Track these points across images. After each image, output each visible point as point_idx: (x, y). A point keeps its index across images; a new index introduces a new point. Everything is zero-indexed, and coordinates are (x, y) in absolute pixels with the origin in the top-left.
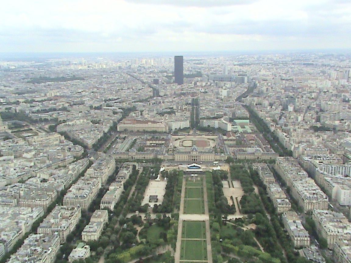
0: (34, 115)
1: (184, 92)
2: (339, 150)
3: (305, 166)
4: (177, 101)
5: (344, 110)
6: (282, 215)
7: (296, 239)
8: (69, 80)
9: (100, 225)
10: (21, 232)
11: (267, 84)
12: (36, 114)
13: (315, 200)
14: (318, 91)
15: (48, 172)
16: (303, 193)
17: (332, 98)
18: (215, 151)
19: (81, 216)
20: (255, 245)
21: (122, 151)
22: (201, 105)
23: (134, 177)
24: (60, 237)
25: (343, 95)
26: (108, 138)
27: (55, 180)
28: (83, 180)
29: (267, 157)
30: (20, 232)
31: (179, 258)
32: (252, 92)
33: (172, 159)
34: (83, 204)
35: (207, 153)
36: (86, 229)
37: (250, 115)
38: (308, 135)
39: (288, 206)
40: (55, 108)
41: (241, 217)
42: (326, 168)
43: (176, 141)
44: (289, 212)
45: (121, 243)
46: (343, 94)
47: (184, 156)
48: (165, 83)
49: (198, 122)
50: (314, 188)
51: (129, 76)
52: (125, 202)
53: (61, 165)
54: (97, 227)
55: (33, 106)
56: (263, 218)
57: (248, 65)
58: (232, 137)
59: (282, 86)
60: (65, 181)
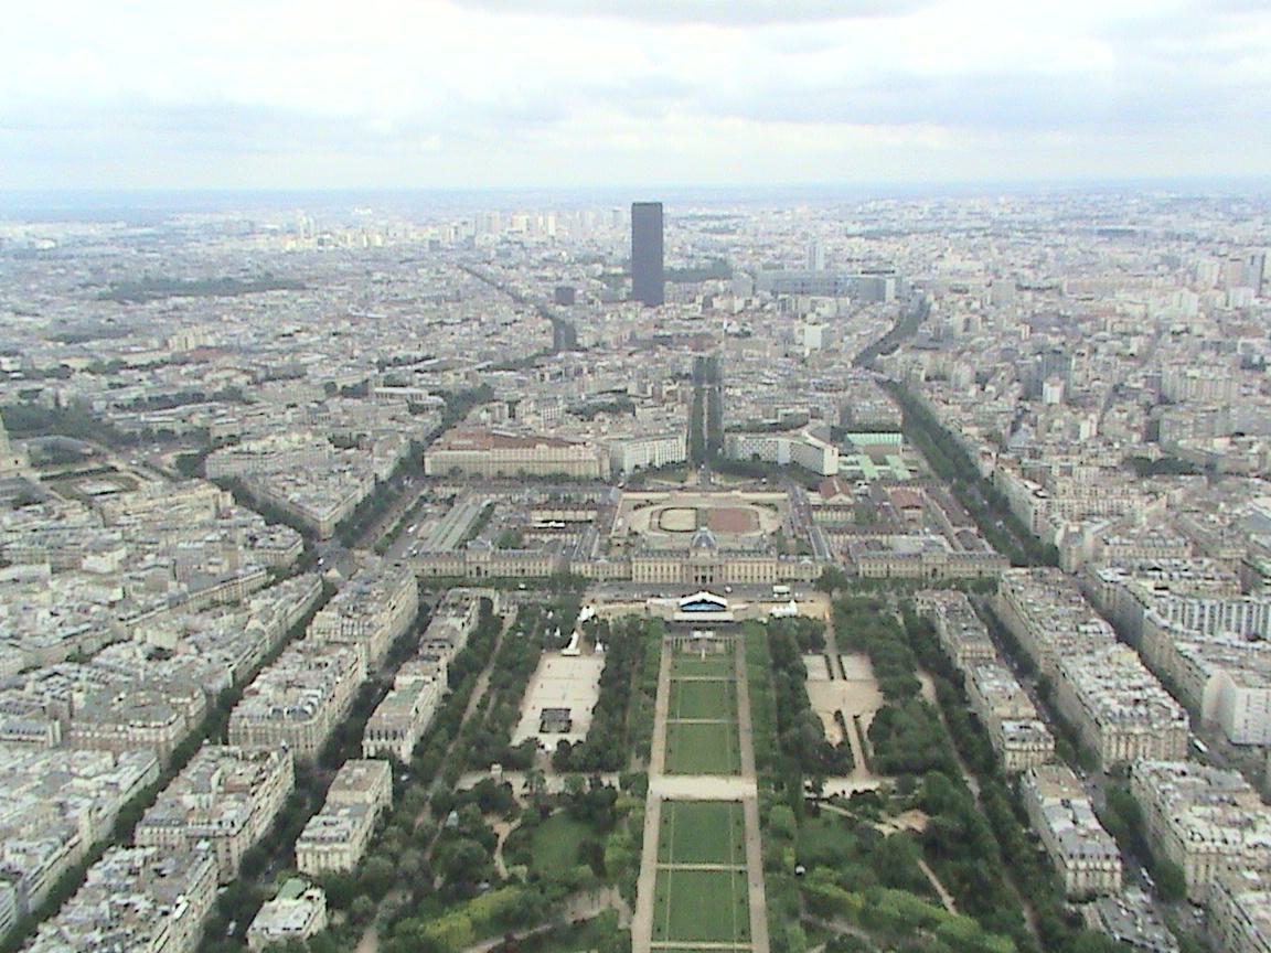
0: (122, 416)
1: (668, 333)
2: (1227, 542)
3: (1104, 600)
4: (640, 366)
5: (1244, 400)
6: (1023, 778)
7: (1071, 864)
8: (249, 289)
9: (363, 815)
10: (75, 840)
11: (969, 304)
12: (131, 415)
13: (1142, 724)
14: (1152, 331)
15: (175, 622)
16: (1099, 700)
17: (1204, 356)
18: (780, 545)
19: (292, 782)
20: (922, 887)
21: (443, 547)
22: (728, 381)
23: (485, 640)
24: (216, 860)
25: (1243, 345)
26: (390, 498)
27: (200, 651)
28: (299, 651)
29: (965, 569)
30: (71, 842)
31: (649, 935)
32: (914, 332)
33: (622, 575)
34: (302, 740)
35: (749, 553)
36: (310, 829)
37: (905, 418)
38: (1117, 490)
39: (1042, 746)
40: (198, 390)
41: (873, 785)
42: (1180, 608)
43: (639, 511)
44: (1045, 767)
45: (439, 881)
46: (1242, 340)
47: (665, 565)
48: (598, 302)
49: (716, 443)
50: (1138, 682)
51: (467, 276)
52: (453, 733)
53: (220, 597)
54: (350, 823)
55: (121, 386)
56: (954, 791)
57: (900, 234)
58: (842, 496)
59: (1020, 312)
60: (237, 656)
